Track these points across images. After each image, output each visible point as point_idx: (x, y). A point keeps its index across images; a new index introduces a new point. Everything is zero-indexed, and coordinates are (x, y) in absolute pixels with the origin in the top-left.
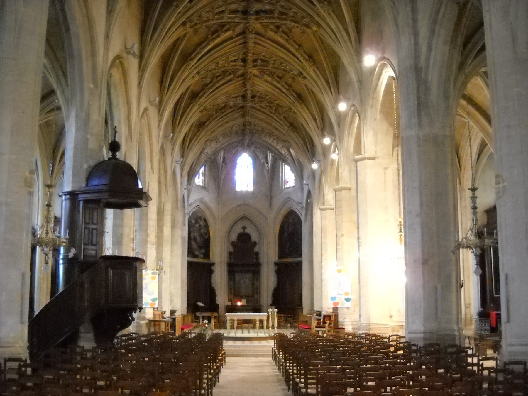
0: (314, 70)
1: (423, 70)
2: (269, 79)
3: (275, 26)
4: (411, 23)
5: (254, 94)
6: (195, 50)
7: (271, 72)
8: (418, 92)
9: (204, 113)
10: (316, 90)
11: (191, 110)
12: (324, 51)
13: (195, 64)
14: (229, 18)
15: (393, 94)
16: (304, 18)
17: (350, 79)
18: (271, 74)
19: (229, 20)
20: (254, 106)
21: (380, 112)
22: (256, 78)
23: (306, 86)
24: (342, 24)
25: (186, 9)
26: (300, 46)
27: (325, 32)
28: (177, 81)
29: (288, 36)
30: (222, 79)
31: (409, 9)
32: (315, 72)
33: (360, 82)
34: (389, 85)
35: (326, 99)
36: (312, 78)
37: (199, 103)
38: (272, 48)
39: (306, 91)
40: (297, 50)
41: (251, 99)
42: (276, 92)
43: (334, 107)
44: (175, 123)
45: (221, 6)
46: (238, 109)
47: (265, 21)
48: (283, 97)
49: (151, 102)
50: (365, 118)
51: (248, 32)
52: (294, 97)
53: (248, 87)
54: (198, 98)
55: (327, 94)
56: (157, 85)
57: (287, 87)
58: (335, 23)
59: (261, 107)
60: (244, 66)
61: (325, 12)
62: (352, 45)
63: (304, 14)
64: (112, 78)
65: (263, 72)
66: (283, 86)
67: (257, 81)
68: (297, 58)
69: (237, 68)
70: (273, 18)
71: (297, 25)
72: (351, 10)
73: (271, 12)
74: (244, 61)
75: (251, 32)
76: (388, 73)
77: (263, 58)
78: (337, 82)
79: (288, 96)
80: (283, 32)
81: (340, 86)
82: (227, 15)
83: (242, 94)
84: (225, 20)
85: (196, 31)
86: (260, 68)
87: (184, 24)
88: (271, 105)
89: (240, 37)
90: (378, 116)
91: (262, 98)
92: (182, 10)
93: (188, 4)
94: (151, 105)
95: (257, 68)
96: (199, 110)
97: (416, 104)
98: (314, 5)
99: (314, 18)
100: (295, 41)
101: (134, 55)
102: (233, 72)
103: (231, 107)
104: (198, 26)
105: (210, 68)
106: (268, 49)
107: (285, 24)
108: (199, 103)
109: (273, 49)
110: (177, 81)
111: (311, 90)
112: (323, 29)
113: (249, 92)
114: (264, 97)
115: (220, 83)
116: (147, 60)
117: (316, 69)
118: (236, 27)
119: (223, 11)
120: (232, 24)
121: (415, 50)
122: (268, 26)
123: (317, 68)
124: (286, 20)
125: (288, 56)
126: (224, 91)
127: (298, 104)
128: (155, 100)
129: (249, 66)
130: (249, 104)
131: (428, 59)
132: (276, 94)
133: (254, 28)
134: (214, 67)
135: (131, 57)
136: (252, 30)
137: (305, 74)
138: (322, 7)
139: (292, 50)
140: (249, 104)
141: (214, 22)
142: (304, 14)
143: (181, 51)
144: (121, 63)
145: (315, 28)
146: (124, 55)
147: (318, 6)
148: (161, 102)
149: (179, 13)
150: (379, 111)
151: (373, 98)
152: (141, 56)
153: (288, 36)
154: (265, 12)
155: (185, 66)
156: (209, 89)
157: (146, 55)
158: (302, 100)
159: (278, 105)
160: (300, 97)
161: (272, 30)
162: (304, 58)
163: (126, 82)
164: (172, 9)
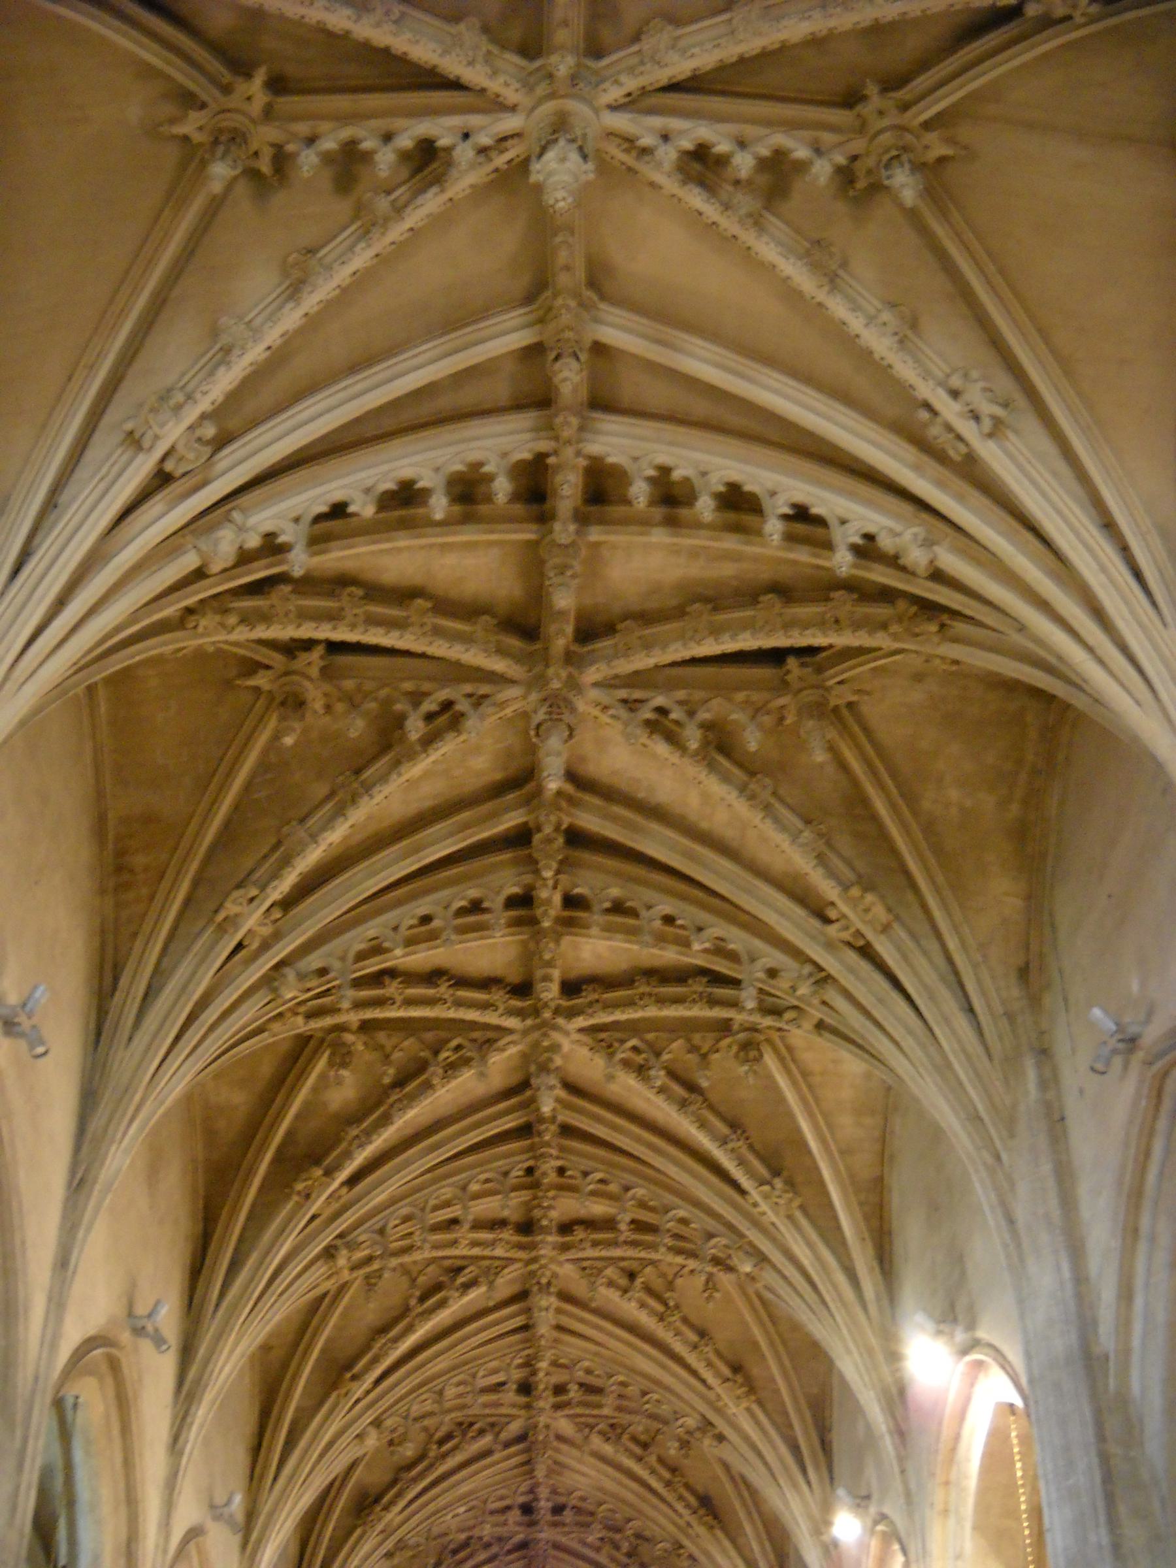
0: (748, 1409)
1: (1111, 1364)
2: (608, 1449)
3: (623, 1270)
4: (1056, 1214)
5: (562, 1500)
6: (367, 1347)
7: (612, 1426)
8: (1101, 1437)
9: (396, 1561)
10: (757, 1477)
11: (352, 1550)
12: (781, 1348)
13: (368, 1392)
14: (474, 1244)
15: (1013, 1464)
16: (711, 1236)
17: (868, 1427)
18: (614, 1432)
19: (476, 1251)
20: (564, 1540)
21: (975, 1528)
22: (564, 1447)
23: (726, 1467)
24: (834, 1252)
25: (336, 1206)
26: (702, 1334)
27: (781, 1282)
28: (306, 1451)
29: (666, 1305)
30: (455, 1448)
31: (1047, 1168)
32: (753, 1415)
33: (901, 1434)
34: (997, 1437)
35: (792, 1505)
36: (747, 1439)
37: (380, 1527)
38: (612, 1343)
39: (729, 1487)
40: (724, 1142)
41: (549, 1517)
42: (629, 1491)
43: (821, 1524)
44: (262, 1477)
45: (447, 1204)
46: (509, 1552)
47: (590, 1253)
48: (655, 1507)
49: (215, 1510)
50: (925, 1552)
51: (535, 1288)
52: (688, 1506)
53: (540, 1472)
54: (379, 1508)
55: (795, 1486)
56: (240, 1456)
57: (667, 1475)
58: (810, 1245)
59: (585, 1544)
60: (528, 1407)
61: (777, 1214)
62: (869, 1318)
63: (712, 1225)
64: (80, 1413)
65: (587, 1425)
66: (653, 1472)
67: (569, 1456)
68: (694, 1373)
69: (504, 1410)
70: (614, 1244)
71: (692, 1264)
72: (861, 1204)
73: (609, 1224)
74: (525, 1388)
75: (545, 1288)
76: (997, 1389)
77: (579, 1504)
78: (826, 1446)
79: (670, 1506)
80: (649, 1290)
81: (836, 1459)
82: (464, 1234)
83: (522, 1499)
84: (462, 1251)
85: (368, 1284)
86: (579, 1410)
87: (329, 1253)
88: (618, 1536)
89: (516, 1555)
90: (969, 1543)
91: (585, 1515)
92: (322, 1208)
93: (344, 1190)
94: (217, 1518)
95: (567, 1412)
96: (383, 1550)
97: (1098, 1479)
98: (743, 1192)
99: (742, 1236)
100: (685, 1320)
101: (159, 1341)
102: (493, 1425)
103: (488, 1546)
104: (376, 1266)
105: (416, 1410)
106: (596, 1350)
107: (652, 1263)
108: (380, 1527)
109: (619, 1344)
110: (306, 1451)
111: (743, 1477)
112: (774, 1267)
113: (543, 1492)
114: (591, 1508)
115: (451, 1463)
116: (207, 1361)
117: (755, 1407)
118: (497, 1274)
119: (454, 1222)
120: (486, 1263)
121: (1080, 1297)
122: (600, 1271)
123: (760, 1403)
124: (652, 1247)
125: (663, 1367)
126: (464, 1488)
127: (701, 1530)
128: (229, 1502)
129: (541, 1404)
130: (546, 1534)
131: (1124, 1324)
132: (630, 1497)
133: (555, 1275)
134: (428, 1406)
135: (146, 1346)
136: (549, 1284)
137: (722, 1426)
138: (766, 1197)
139: (678, 1347)
140: (546, 1534)
141: (427, 1254)
142: (712, 1225)
143: (323, 1351)
144: (114, 1365)
145: (747, 1268)
146: (125, 1337)
147: (755, 1195)
148: (251, 1515)
149: (314, 1217)
150: (968, 1525)
151: (947, 1483)
152: (187, 1352)
153: (666, 1305)
154: (590, 1224)
155: (334, 1395)
156: (415, 1480)
157: (202, 1351)
158: (716, 1517)
159: (638, 1536)
160: (708, 1506)
161: (611, 1284)
162: (718, 1374)
163: (126, 1429)
164: (290, 1205)
